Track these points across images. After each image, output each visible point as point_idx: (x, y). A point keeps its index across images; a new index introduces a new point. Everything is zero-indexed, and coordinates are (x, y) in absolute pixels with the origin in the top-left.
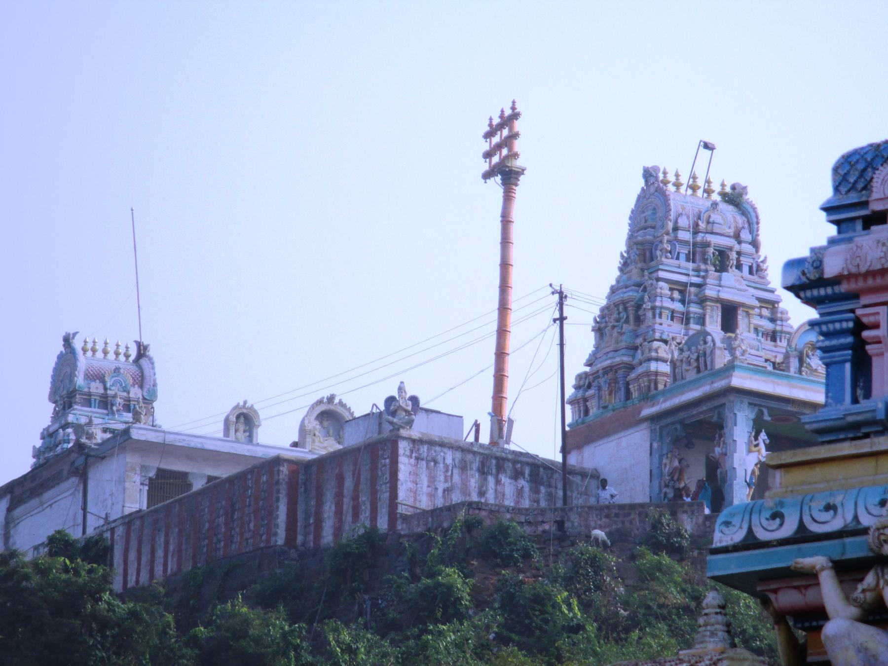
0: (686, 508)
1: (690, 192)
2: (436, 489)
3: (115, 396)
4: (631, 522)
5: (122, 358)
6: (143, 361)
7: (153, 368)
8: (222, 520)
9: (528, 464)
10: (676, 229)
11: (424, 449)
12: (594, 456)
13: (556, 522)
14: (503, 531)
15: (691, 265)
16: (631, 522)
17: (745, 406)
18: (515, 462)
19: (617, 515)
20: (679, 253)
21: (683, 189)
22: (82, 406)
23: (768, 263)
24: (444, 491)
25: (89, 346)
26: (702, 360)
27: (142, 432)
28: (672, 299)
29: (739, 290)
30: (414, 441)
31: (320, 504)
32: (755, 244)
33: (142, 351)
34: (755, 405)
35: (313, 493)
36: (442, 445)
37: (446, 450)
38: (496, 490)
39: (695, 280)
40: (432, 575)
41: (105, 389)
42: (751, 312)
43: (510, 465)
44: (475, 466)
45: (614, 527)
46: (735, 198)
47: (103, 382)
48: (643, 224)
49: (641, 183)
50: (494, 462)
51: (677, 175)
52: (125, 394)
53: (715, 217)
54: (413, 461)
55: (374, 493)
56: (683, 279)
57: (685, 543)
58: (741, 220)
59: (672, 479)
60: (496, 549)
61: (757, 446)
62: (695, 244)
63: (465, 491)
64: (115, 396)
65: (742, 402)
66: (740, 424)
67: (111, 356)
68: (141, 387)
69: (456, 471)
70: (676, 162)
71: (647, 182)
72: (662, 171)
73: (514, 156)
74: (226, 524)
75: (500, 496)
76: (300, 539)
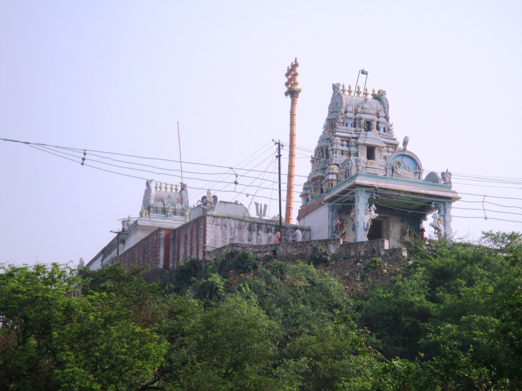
0: (332, 241)
1: (356, 94)
2: (226, 239)
3: (168, 208)
4: (307, 250)
5: (174, 191)
6: (183, 192)
7: (187, 195)
8: (141, 258)
9: (274, 225)
10: (346, 112)
11: (219, 221)
12: (310, 221)
13: (273, 251)
14: (245, 256)
15: (353, 129)
16: (307, 250)
17: (364, 192)
18: (266, 225)
19: (300, 247)
20: (347, 124)
21: (352, 94)
22: (154, 213)
23: (393, 126)
24: (230, 239)
25: (158, 186)
26: (347, 172)
27: (143, 221)
28: (343, 145)
29: (375, 139)
30: (214, 217)
31: (179, 248)
32: (387, 118)
33: (183, 187)
34: (369, 192)
35: (176, 244)
36: (229, 218)
37: (231, 220)
38: (257, 238)
39: (354, 135)
40: (206, 278)
41: (164, 205)
42: (382, 149)
43: (264, 226)
44: (247, 227)
45: (299, 252)
46: (379, 97)
47: (163, 202)
48: (332, 111)
49: (332, 92)
50: (256, 225)
51: (350, 87)
52: (173, 207)
53: (366, 106)
54: (214, 226)
55: (198, 242)
56: (349, 135)
57: (329, 258)
58: (380, 107)
59: (337, 229)
60: (240, 264)
61: (370, 211)
62: (355, 119)
63: (241, 239)
64: (168, 208)
65: (362, 190)
66: (362, 202)
67: (169, 190)
68: (182, 204)
69: (236, 230)
70: (349, 80)
71: (334, 91)
72: (341, 85)
73: (296, 84)
74: (143, 260)
75: (259, 241)
76: (171, 265)
